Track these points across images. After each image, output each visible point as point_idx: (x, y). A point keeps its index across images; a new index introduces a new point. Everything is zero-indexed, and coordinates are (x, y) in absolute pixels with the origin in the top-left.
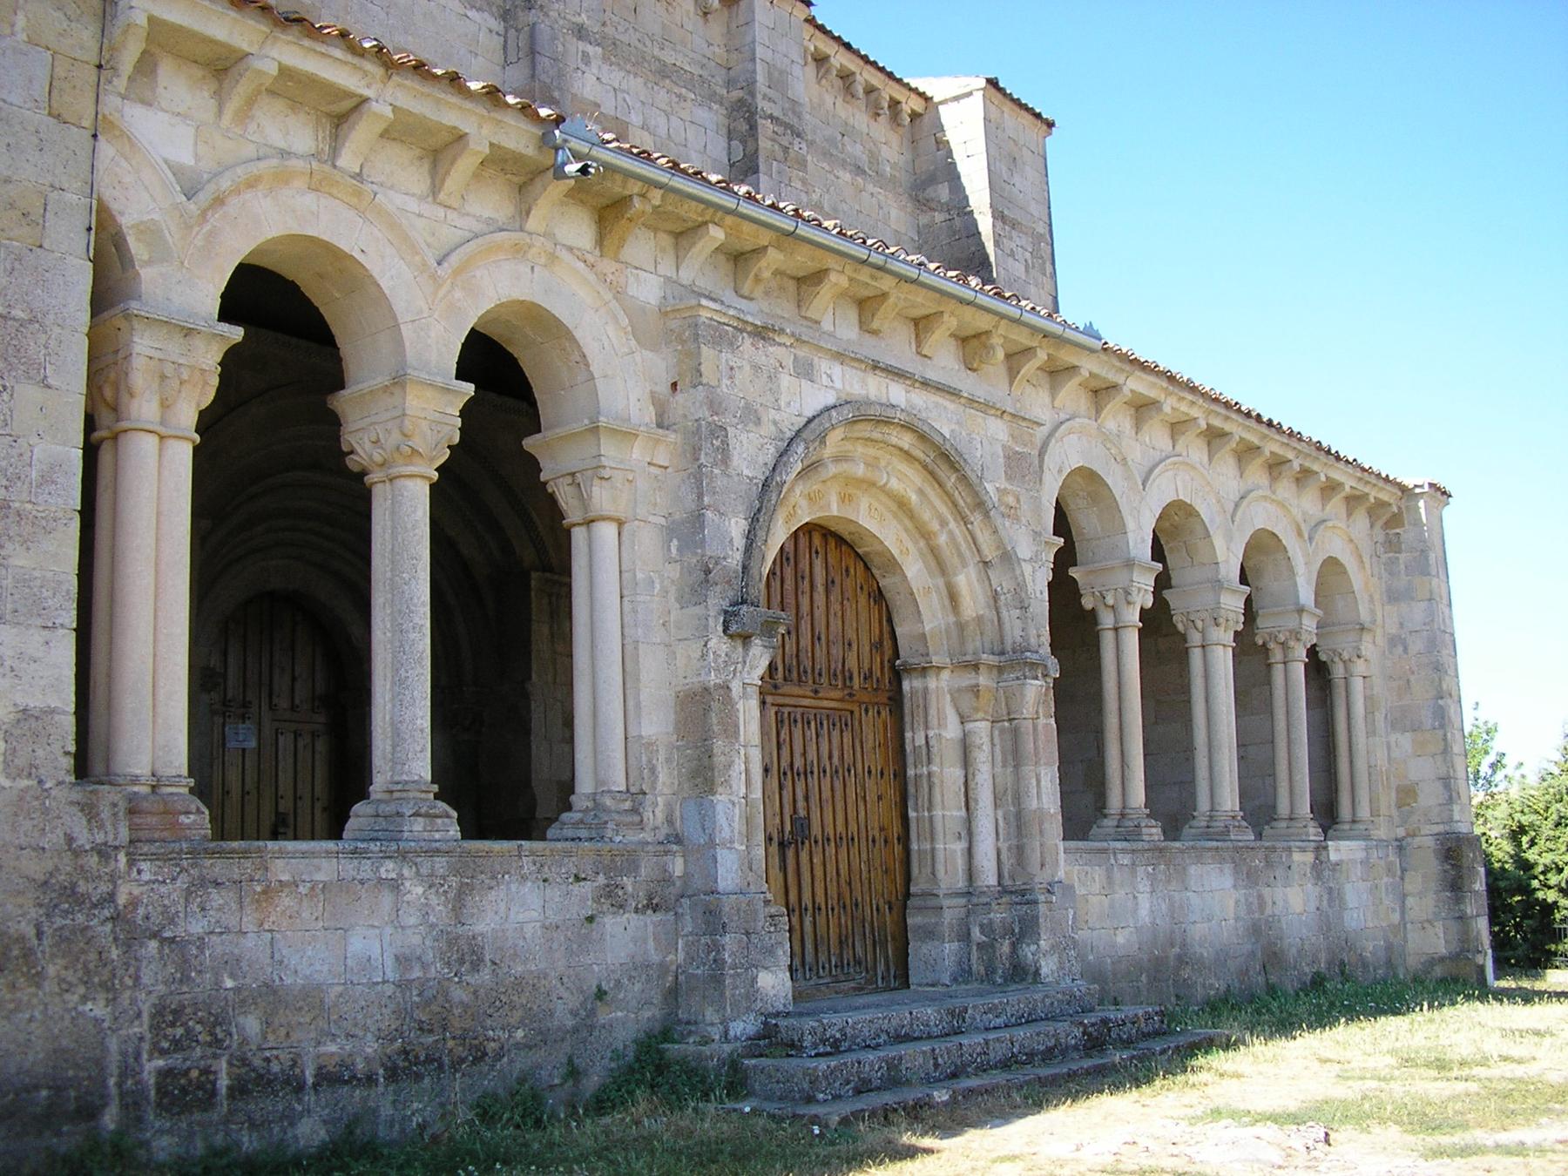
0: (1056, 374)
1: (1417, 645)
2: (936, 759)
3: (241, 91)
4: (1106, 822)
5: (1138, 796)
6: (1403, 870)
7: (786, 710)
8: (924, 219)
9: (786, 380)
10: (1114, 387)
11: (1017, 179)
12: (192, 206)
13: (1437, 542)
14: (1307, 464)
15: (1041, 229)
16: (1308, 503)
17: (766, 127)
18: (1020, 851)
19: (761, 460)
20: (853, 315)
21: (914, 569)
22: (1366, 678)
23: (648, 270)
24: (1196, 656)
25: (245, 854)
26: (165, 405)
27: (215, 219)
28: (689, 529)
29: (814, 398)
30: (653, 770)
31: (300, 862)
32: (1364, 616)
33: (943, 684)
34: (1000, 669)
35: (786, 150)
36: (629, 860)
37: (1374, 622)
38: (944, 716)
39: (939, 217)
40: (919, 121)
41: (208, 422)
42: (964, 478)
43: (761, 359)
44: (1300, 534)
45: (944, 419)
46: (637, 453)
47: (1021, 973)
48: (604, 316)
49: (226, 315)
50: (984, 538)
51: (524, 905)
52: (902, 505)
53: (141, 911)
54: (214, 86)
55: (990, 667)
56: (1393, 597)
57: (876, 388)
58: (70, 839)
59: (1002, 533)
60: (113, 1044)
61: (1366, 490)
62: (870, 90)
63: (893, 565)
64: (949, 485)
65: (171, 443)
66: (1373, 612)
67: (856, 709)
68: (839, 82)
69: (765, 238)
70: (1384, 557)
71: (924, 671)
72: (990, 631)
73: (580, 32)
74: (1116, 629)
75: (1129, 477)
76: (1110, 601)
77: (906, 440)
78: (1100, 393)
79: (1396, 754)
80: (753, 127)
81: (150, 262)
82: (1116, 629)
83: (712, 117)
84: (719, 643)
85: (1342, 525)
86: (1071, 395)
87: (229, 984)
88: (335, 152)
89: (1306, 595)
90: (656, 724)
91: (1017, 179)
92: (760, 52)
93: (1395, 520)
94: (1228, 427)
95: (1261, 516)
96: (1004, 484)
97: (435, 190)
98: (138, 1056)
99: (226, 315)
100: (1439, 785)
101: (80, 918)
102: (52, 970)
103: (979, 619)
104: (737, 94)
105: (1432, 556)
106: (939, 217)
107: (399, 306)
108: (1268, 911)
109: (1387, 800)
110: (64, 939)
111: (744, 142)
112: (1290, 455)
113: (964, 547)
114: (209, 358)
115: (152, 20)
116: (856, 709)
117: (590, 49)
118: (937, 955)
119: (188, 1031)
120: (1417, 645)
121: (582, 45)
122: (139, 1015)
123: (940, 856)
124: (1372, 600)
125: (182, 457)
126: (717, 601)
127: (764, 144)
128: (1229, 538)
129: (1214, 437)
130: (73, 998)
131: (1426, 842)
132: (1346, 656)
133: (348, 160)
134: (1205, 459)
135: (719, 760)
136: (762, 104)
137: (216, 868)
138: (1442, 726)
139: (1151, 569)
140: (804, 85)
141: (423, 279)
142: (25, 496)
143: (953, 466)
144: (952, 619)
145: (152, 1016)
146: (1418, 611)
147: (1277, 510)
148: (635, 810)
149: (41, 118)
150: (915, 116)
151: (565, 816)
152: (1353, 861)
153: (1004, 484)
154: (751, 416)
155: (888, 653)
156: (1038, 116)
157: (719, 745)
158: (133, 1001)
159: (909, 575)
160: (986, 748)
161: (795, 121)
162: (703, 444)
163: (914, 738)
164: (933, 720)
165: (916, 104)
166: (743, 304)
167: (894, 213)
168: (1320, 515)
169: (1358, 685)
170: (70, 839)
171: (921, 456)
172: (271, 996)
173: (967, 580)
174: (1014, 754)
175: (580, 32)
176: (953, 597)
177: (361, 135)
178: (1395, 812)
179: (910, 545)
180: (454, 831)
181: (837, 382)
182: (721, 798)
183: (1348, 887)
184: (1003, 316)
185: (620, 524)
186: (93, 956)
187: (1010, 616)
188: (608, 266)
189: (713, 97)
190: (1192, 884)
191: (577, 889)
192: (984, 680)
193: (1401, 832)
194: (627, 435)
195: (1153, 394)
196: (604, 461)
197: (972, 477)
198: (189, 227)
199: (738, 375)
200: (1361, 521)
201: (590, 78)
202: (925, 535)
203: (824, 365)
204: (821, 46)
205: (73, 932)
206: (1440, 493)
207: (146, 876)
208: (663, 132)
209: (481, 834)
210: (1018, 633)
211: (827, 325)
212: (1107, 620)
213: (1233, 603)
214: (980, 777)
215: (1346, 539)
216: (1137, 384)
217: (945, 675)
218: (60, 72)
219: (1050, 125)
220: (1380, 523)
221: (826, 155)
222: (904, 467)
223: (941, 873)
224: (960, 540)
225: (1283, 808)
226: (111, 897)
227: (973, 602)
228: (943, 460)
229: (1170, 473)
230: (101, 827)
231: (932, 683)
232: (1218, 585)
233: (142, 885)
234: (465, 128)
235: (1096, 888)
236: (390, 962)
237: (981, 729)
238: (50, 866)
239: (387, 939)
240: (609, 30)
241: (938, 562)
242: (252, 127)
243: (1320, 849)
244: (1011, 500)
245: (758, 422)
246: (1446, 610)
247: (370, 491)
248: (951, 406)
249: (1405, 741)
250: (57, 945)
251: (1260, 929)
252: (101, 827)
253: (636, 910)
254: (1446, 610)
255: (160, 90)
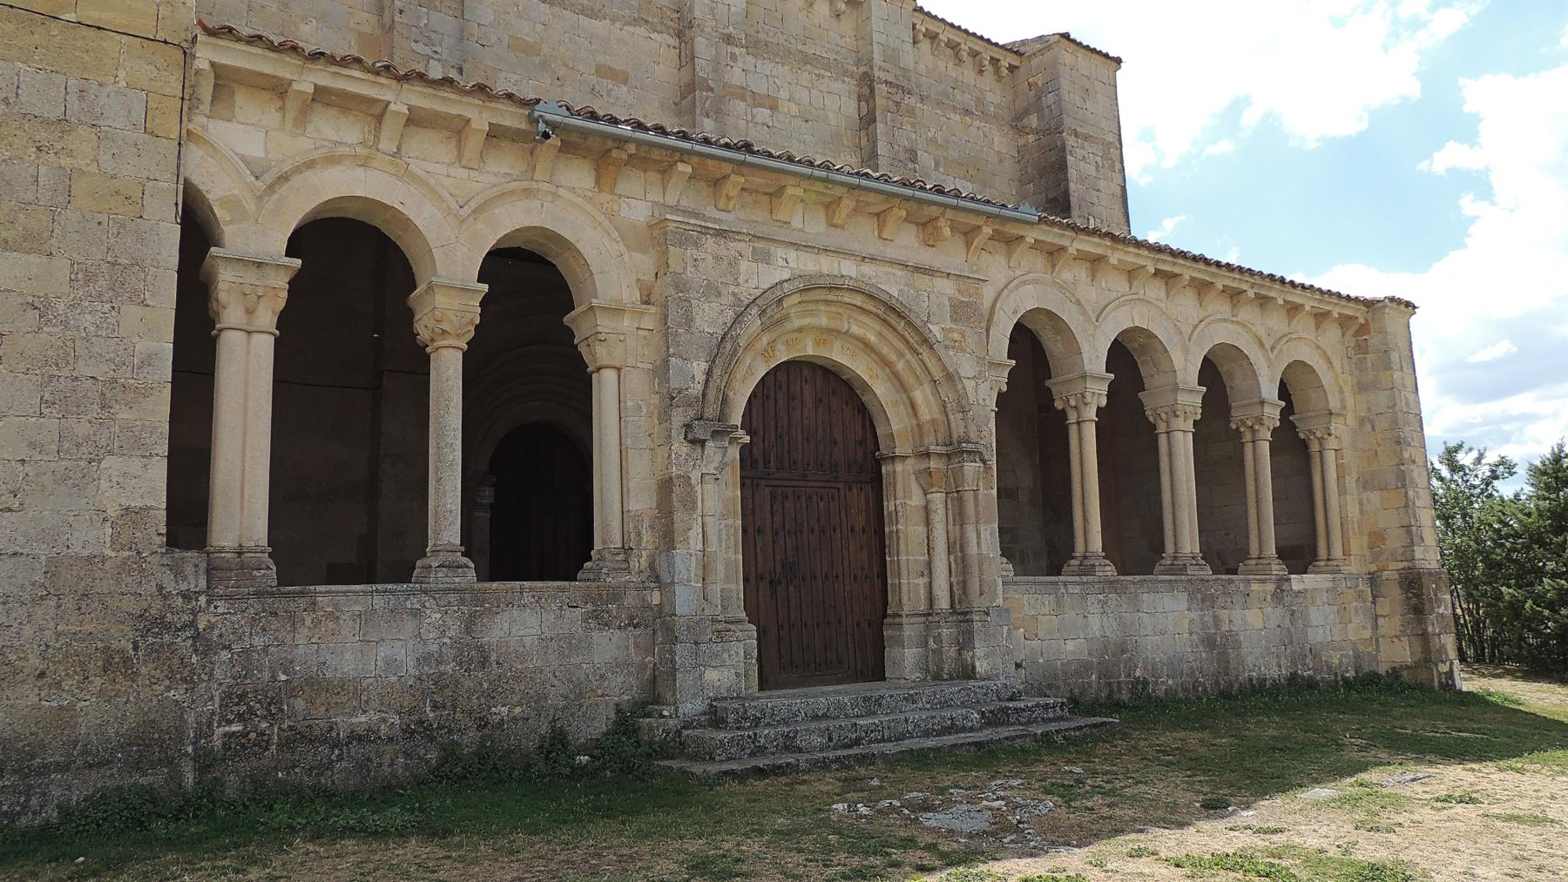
1: (1382, 424)
2: (901, 520)
3: (292, 104)
4: (1073, 562)
5: (1097, 543)
6: (1375, 597)
7: (779, 491)
8: (1021, 142)
9: (744, 265)
10: (1062, 249)
11: (1089, 105)
12: (259, 184)
13: (1402, 344)
14: (1263, 292)
15: (1111, 138)
16: (1276, 322)
17: (882, 90)
18: (964, 585)
19: (721, 321)
20: (821, 215)
21: (881, 389)
22: (1340, 450)
23: (638, 200)
24: (1163, 439)
25: (302, 594)
26: (250, 312)
27: (282, 191)
30: (639, 534)
31: (353, 599)
32: (1334, 404)
33: (910, 468)
34: (948, 456)
35: (898, 104)
36: (616, 595)
37: (1344, 407)
38: (907, 495)
39: (1031, 138)
41: (283, 320)
42: (910, 324)
43: (723, 252)
44: (1262, 345)
45: (893, 285)
46: (627, 323)
47: (968, 673)
48: (601, 230)
49: (290, 253)
50: (932, 364)
51: (529, 624)
53: (216, 632)
54: (280, 103)
55: (940, 455)
57: (826, 265)
58: (160, 588)
59: (946, 360)
60: (191, 718)
61: (1328, 308)
62: (974, 54)
63: (866, 387)
64: (899, 328)
65: (256, 337)
66: (1343, 400)
67: (841, 486)
68: (949, 52)
69: (728, 168)
70: (1355, 359)
71: (893, 458)
72: (942, 429)
74: (1078, 423)
75: (1084, 313)
76: (1073, 403)
77: (858, 300)
79: (1367, 507)
80: (872, 90)
81: (231, 222)
82: (1078, 423)
84: (680, 447)
85: (1312, 337)
87: (283, 678)
88: (377, 138)
90: (642, 502)
91: (1089, 105)
92: (876, 37)
93: (1363, 329)
94: (1177, 270)
96: (949, 325)
97: (460, 157)
98: (210, 725)
99: (290, 253)
100: (1402, 531)
101: (167, 638)
102: (144, 670)
103: (933, 421)
104: (862, 69)
105: (1394, 356)
107: (430, 236)
108: (1225, 627)
109: (1358, 545)
110: (155, 651)
111: (867, 102)
112: (1244, 287)
113: (919, 371)
114: (281, 282)
115: (213, 64)
116: (841, 486)
117: (736, 50)
118: (906, 657)
119: (250, 709)
120: (1382, 424)
121: (730, 49)
122: (212, 698)
123: (904, 588)
124: (1341, 391)
125: (264, 347)
126: (679, 418)
127: (880, 101)
128: (1186, 351)
130: (159, 688)
131: (1391, 572)
132: (1319, 434)
133: (387, 145)
134: (1163, 295)
135: (678, 526)
136: (877, 73)
137: (279, 605)
138: (1404, 486)
139: (1103, 379)
141: (454, 217)
142: (129, 375)
143: (900, 315)
144: (914, 422)
145: (222, 700)
146: (1382, 399)
148: (626, 561)
149: (140, 136)
150: (1012, 68)
151: (587, 565)
152: (1321, 590)
153: (949, 325)
154: (712, 291)
155: (871, 447)
156: (1106, 56)
157: (679, 516)
158: (208, 689)
159: (878, 393)
160: (941, 511)
161: (905, 83)
163: (889, 506)
164: (900, 494)
166: (723, 215)
167: (996, 139)
168: (1287, 330)
169: (1330, 456)
170: (160, 588)
171: (873, 309)
172: (315, 685)
173: (922, 395)
174: (959, 517)
177: (391, 127)
178: (1367, 553)
179: (879, 372)
180: (471, 575)
182: (679, 551)
183: (1312, 609)
184: (946, 206)
185: (619, 370)
186: (176, 661)
187: (956, 418)
188: (605, 197)
189: (845, 73)
190: (1145, 607)
191: (568, 613)
192: (934, 464)
193: (1373, 568)
194: (617, 311)
195: (1099, 251)
196: (600, 329)
197: (918, 323)
198: (260, 198)
199: (702, 265)
200: (1332, 334)
201: (737, 71)
202: (886, 363)
204: (931, 28)
205: (162, 646)
206: (1410, 306)
207: (220, 610)
208: (806, 101)
209: (492, 579)
210: (962, 430)
211: (797, 223)
212: (1072, 417)
214: (940, 530)
217: (908, 461)
218: (152, 104)
219: (1118, 61)
220: (1351, 332)
221: (939, 104)
222: (864, 318)
223: (905, 601)
224: (915, 365)
225: (1254, 552)
226: (193, 624)
228: (891, 312)
229: (1127, 308)
230: (185, 578)
231: (899, 467)
233: (215, 616)
234: (467, 114)
235: (1046, 609)
236: (411, 663)
237: (938, 498)
238: (145, 605)
239: (410, 646)
240: (762, 36)
242: (310, 128)
243: (1282, 580)
244: (956, 336)
245: (719, 295)
246: (1412, 397)
247: (428, 357)
248: (900, 273)
249: (1374, 497)
250: (149, 655)
251: (1217, 643)
252: (185, 578)
253: (620, 627)
254: (1412, 397)
255: (237, 110)
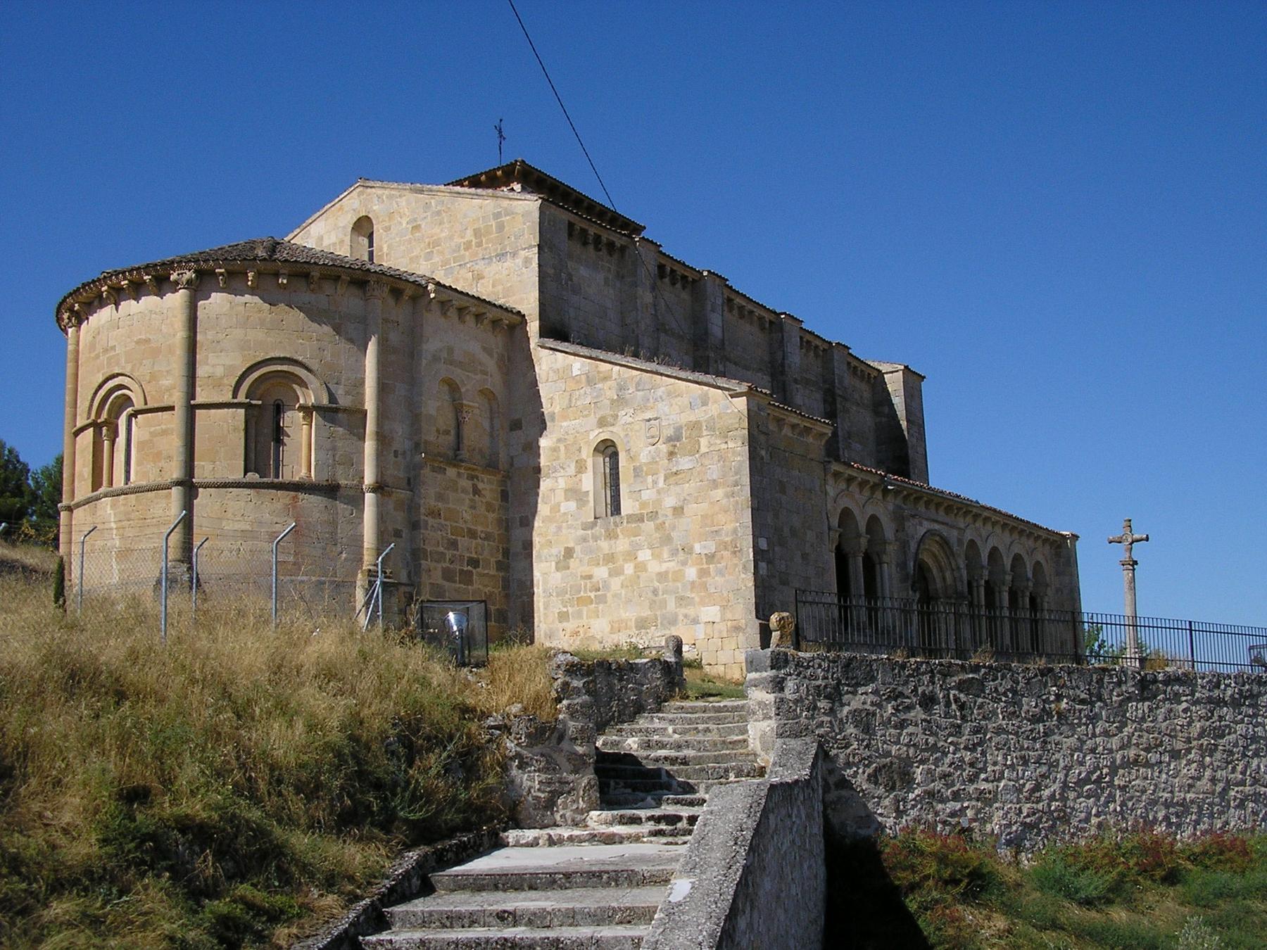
0: (966, 513)
17: (839, 399)
21: (935, 571)
22: (1049, 600)
28: (902, 565)
29: (922, 531)
40: (876, 381)
45: (945, 531)
52: (934, 555)
56: (1058, 574)
63: (929, 570)
73: (796, 381)
78: (976, 516)
83: (818, 396)
86: (969, 519)
89: (1030, 575)
92: (837, 371)
93: (1059, 547)
95: (1017, 549)
106: (884, 420)
126: (910, 582)
129: (1005, 525)
140: (848, 380)
147: (1021, 547)
162: (904, 545)
165: (875, 374)
173: (948, 574)
175: (796, 381)
176: (944, 579)
181: (927, 525)
187: (959, 584)
203: (925, 522)
213: (1009, 578)
215: (1042, 554)
216: (986, 514)
227: (949, 580)
232: (1005, 573)
241: (941, 570)
